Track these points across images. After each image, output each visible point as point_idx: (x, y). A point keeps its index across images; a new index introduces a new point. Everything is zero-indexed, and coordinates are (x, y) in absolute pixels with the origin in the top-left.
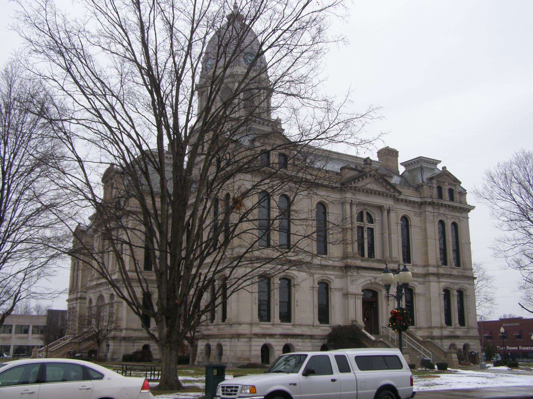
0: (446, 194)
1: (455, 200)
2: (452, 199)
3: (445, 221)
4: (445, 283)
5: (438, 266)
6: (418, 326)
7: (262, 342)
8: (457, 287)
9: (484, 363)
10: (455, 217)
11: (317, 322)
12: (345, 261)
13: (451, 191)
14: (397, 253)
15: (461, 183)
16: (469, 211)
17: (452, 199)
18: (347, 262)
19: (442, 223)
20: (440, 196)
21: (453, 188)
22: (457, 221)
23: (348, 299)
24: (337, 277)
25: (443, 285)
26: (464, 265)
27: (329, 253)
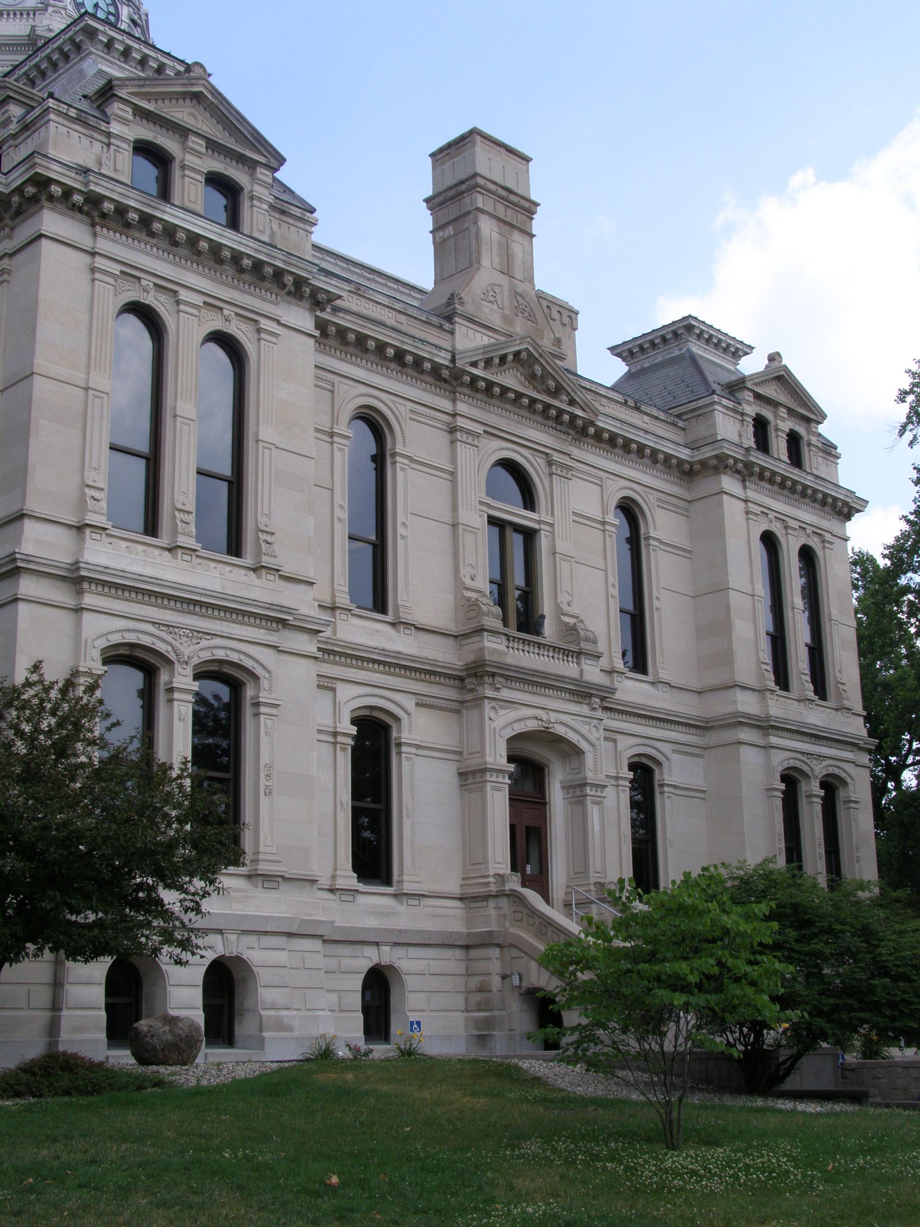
0: (780, 446)
1: (246, 226)
2: (796, 458)
3: (782, 539)
4: (786, 751)
5: (761, 691)
6: (408, 887)
7: (367, 958)
8: (819, 769)
9: (858, 1044)
10: (228, 311)
11: (349, 879)
12: (472, 645)
13: (794, 440)
14: (604, 625)
15: (281, 160)
16: (848, 517)
17: (796, 458)
18: (482, 650)
19: (769, 540)
20: (763, 443)
21: (801, 430)
22: (815, 543)
23: (482, 790)
24: (681, 748)
25: (780, 761)
26: (259, 552)
27: (396, 606)
